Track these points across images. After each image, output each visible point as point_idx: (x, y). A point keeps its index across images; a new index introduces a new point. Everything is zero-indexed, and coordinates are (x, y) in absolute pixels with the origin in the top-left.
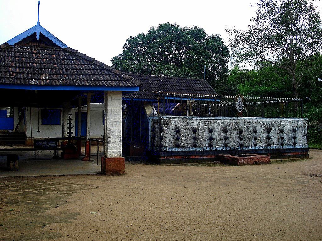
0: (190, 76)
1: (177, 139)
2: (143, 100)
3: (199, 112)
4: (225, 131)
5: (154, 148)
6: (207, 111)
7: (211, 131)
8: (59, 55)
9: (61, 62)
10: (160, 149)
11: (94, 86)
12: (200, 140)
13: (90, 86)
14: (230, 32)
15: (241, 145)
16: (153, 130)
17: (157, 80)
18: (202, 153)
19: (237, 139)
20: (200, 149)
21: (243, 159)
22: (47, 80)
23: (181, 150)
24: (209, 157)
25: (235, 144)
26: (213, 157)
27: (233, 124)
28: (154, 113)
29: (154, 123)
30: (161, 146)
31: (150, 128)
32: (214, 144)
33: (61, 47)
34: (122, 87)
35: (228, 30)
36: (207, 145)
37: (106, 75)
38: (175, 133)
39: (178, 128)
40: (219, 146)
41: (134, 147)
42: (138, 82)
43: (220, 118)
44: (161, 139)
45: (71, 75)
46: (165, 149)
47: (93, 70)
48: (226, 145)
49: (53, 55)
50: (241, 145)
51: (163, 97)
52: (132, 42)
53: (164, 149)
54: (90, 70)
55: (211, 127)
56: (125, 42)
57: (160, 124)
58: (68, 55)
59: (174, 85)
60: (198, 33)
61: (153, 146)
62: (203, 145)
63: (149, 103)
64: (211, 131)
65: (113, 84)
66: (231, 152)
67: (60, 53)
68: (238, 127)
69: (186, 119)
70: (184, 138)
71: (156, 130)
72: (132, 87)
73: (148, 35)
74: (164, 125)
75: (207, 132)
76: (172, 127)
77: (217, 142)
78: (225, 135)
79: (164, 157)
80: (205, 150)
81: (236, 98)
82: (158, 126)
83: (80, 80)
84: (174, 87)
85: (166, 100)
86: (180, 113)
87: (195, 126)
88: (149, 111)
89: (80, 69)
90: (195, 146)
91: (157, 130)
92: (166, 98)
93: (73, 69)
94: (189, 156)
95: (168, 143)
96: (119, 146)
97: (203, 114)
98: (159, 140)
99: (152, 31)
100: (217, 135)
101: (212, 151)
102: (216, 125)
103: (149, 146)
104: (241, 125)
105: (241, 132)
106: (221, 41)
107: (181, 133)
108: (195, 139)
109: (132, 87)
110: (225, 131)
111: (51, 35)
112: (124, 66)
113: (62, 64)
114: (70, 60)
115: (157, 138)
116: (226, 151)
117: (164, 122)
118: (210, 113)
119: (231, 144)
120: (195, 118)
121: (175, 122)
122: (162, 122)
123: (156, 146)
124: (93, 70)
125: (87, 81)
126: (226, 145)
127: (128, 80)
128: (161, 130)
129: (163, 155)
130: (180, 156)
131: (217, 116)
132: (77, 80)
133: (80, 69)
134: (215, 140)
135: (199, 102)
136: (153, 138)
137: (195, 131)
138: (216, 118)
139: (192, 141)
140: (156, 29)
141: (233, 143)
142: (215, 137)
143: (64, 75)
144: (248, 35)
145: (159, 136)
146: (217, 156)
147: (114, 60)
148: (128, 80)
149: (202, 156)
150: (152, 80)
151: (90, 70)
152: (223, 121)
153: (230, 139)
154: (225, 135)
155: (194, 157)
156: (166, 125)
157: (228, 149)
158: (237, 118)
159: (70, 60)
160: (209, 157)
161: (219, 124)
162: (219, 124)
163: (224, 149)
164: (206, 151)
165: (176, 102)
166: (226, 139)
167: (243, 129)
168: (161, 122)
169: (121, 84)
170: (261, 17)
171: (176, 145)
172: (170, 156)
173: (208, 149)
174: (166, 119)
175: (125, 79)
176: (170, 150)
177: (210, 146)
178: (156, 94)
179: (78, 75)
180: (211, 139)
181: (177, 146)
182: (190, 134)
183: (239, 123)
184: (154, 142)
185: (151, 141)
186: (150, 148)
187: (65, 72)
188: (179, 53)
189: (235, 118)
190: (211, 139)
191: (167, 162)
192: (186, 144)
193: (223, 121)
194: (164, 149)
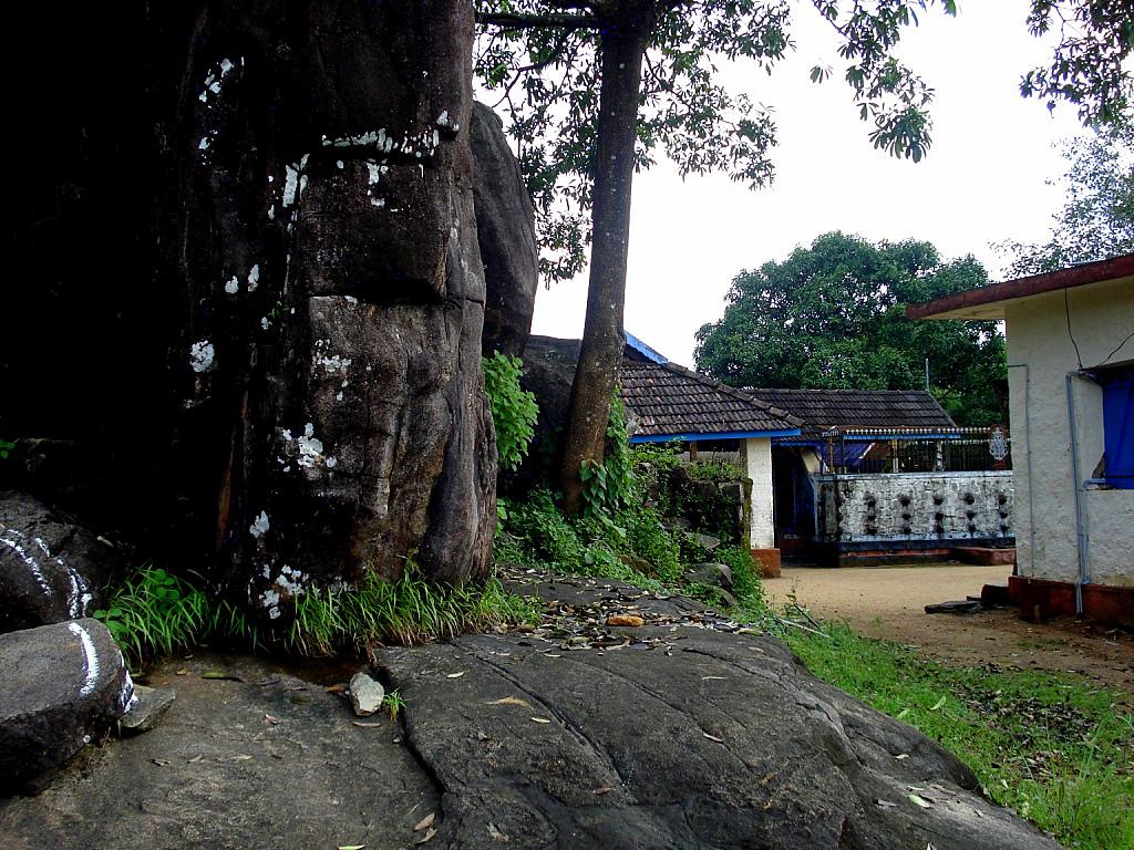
0: (901, 369)
1: (872, 518)
2: (799, 444)
3: (917, 460)
4: (969, 499)
5: (827, 538)
6: (933, 459)
7: (938, 501)
8: (658, 378)
9: (665, 391)
10: (839, 539)
11: (728, 432)
12: (916, 520)
13: (722, 432)
14: (1002, 250)
15: (1004, 529)
16: (822, 503)
17: (823, 401)
18: (922, 545)
19: (994, 517)
20: (917, 538)
21: (1002, 552)
22: (653, 426)
23: (879, 539)
24: (937, 552)
25: (992, 526)
26: (945, 552)
27: (984, 486)
28: (821, 469)
29: (824, 488)
30: (840, 532)
31: (816, 499)
32: (947, 527)
33: (659, 362)
34: (772, 430)
35: (996, 245)
36: (931, 529)
37: (743, 410)
38: (867, 507)
39: (872, 497)
40: (957, 531)
41: (785, 537)
42: (798, 421)
43: (956, 474)
44: (839, 518)
45: (688, 414)
46: (848, 537)
47: (721, 402)
48: (972, 529)
49: (647, 378)
50: (1004, 529)
51: (841, 436)
52: (747, 284)
53: (844, 538)
54: (715, 402)
55: (939, 492)
56: (730, 285)
57: (837, 491)
58: (673, 377)
59: (860, 409)
60: (916, 255)
61: (823, 533)
62: (924, 529)
63: (811, 449)
64: (938, 501)
65: (757, 425)
66: (982, 542)
67: (659, 374)
68: (997, 491)
69: (887, 478)
70: (884, 517)
71: (828, 502)
72: (789, 429)
73: (788, 265)
74: (845, 492)
75: (930, 502)
76: (861, 495)
77: (952, 524)
78: (969, 508)
79: (846, 553)
80: (927, 538)
81: (991, 431)
82: (833, 494)
83: (704, 423)
84: (862, 413)
85: (846, 441)
86: (875, 466)
87: (906, 493)
88: (812, 465)
89: (699, 403)
90: (907, 531)
91: (830, 501)
92: (845, 438)
93: (688, 404)
94: (895, 551)
95: (854, 527)
96: (770, 530)
97: (926, 467)
98: (835, 521)
99: (799, 256)
100: (952, 508)
101: (941, 541)
102: (948, 488)
103: (814, 535)
104: (1002, 488)
105: (1002, 500)
106: (980, 271)
107: (877, 506)
108: (906, 517)
109: (789, 429)
110: (969, 499)
111: (640, 343)
112: (733, 349)
113: (666, 395)
114: (678, 386)
115: (830, 519)
116: (973, 540)
117: (844, 486)
118: (939, 463)
119: (982, 527)
120: (905, 476)
121: (865, 485)
122: (840, 488)
123: (829, 535)
124: (721, 402)
125: (715, 423)
126: (972, 529)
127: (781, 418)
128: (839, 502)
129: (844, 549)
130: (878, 551)
131: (951, 470)
132: (700, 423)
133: (699, 403)
134: (949, 519)
135: (920, 441)
136: (823, 518)
137: (905, 501)
138: (948, 474)
139: (902, 521)
140: (810, 248)
141: (987, 524)
142: (947, 512)
143: (676, 415)
144: (1050, 252)
145: (834, 512)
146: (953, 550)
147: (714, 342)
148: (781, 418)
149: (923, 550)
150: (815, 401)
151: (715, 402)
152: (963, 480)
153: (980, 516)
154: (969, 508)
155: (905, 553)
156: (848, 491)
157: (975, 536)
158: (993, 474)
159: (678, 386)
160: (937, 552)
161: (954, 487)
162: (954, 487)
163: (969, 536)
164: (930, 541)
165: (869, 442)
166: (971, 515)
167: (1006, 494)
168: (837, 486)
169: (770, 425)
170: (1078, 213)
171: (869, 530)
172: (858, 552)
173: (934, 537)
174: (847, 481)
175: (776, 417)
176: (858, 539)
177: (939, 530)
178: (825, 431)
179: (699, 414)
180: (939, 517)
181: (871, 532)
182: (896, 507)
183: (998, 482)
184: (824, 526)
185: (819, 526)
186: (816, 539)
187: (677, 411)
188: (872, 303)
189: (987, 473)
190: (939, 517)
191: (853, 563)
192: (889, 528)
193: (964, 480)
194: (844, 538)
